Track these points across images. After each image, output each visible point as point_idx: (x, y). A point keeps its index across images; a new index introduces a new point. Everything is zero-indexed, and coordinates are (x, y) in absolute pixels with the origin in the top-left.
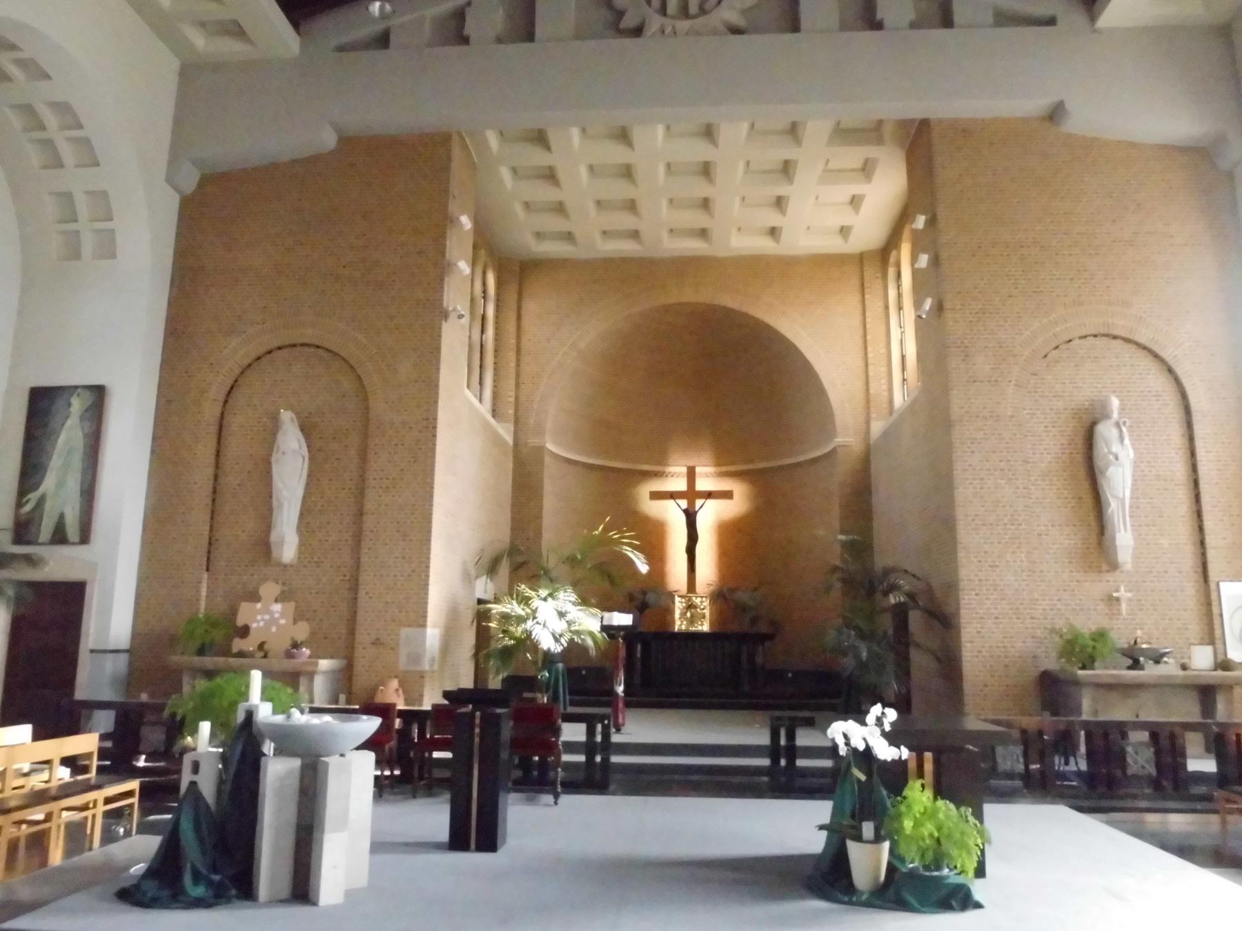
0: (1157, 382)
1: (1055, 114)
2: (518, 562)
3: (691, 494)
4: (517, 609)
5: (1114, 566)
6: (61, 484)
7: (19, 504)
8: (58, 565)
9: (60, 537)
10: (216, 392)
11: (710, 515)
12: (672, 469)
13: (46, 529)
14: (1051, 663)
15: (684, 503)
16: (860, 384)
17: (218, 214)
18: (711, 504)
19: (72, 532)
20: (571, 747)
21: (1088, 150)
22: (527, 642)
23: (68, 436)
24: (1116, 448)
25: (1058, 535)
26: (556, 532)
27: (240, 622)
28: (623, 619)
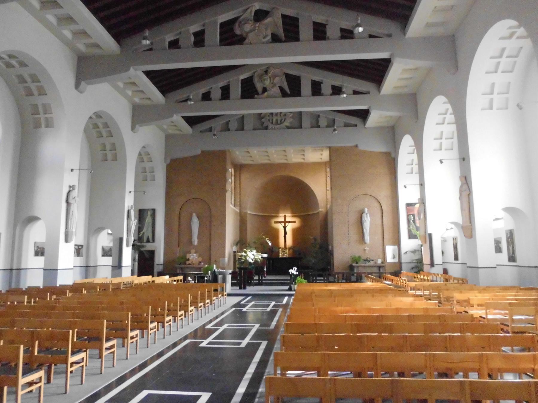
0: (376, 204)
1: (356, 146)
2: (242, 243)
3: (285, 222)
4: (243, 254)
5: (365, 243)
6: (147, 230)
7: (139, 234)
8: (149, 247)
9: (148, 241)
10: (177, 210)
11: (290, 227)
12: (280, 215)
13: (145, 240)
14: (350, 263)
15: (283, 224)
16: (325, 195)
17: (175, 168)
18: (290, 224)
19: (151, 240)
20: (256, 280)
21: (364, 153)
22: (246, 261)
23: (148, 220)
24: (366, 219)
25: (354, 237)
26: (250, 236)
27: (187, 258)
28: (265, 255)
